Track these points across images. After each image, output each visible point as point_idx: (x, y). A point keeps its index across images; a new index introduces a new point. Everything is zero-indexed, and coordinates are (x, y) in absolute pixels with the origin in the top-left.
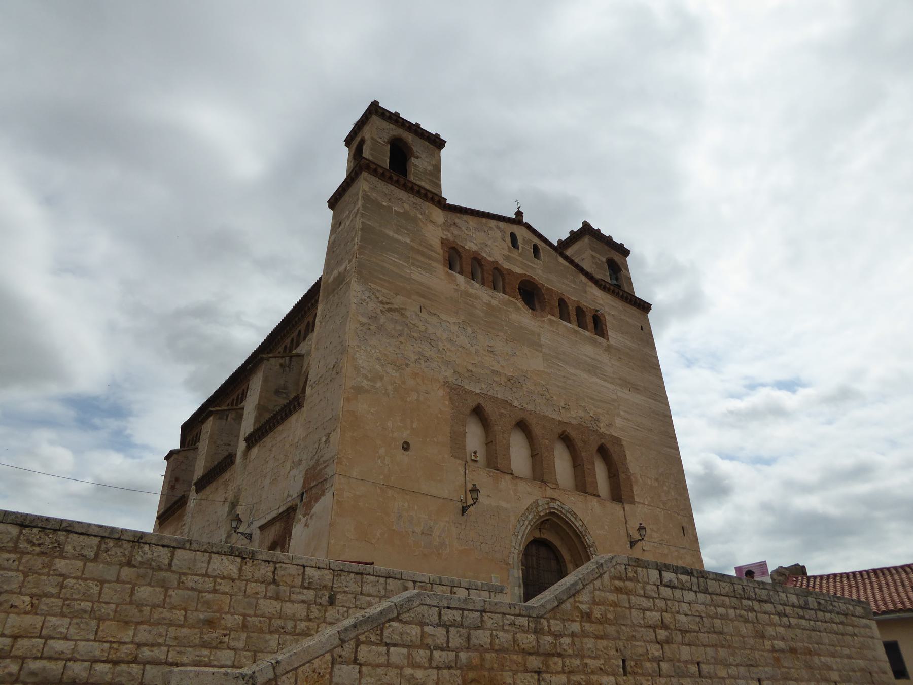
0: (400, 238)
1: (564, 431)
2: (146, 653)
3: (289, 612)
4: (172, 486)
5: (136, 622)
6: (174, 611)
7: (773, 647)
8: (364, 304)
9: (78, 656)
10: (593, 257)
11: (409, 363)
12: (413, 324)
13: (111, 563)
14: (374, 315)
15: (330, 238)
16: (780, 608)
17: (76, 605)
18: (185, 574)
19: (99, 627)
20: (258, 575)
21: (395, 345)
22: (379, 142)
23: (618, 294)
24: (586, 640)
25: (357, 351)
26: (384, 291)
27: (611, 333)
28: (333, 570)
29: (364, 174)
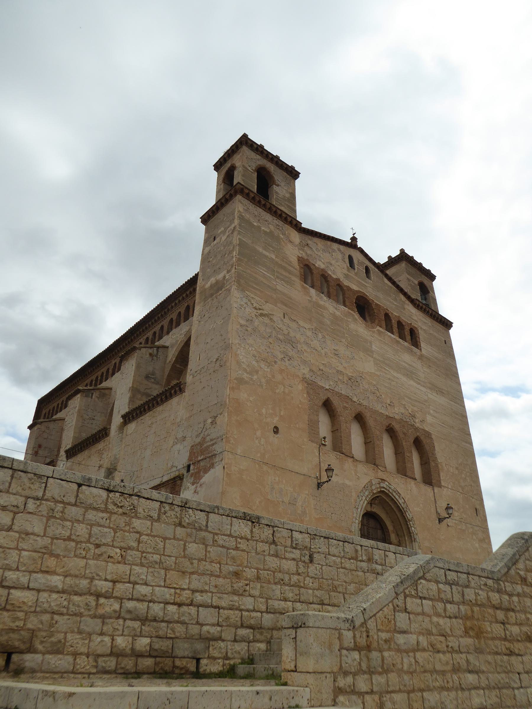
0: (267, 254)
1: (390, 424)
2: (199, 598)
3: (286, 567)
4: (35, 451)
5: (189, 572)
6: (214, 565)
8: (243, 309)
9: (156, 599)
11: (277, 360)
12: (279, 328)
13: (169, 523)
14: (251, 319)
15: (203, 250)
17: (150, 557)
18: (217, 534)
19: (166, 575)
20: (263, 537)
21: (266, 345)
22: (250, 171)
23: (428, 312)
24: (526, 599)
25: (238, 348)
26: (257, 298)
27: (423, 345)
28: (310, 534)
29: (239, 197)
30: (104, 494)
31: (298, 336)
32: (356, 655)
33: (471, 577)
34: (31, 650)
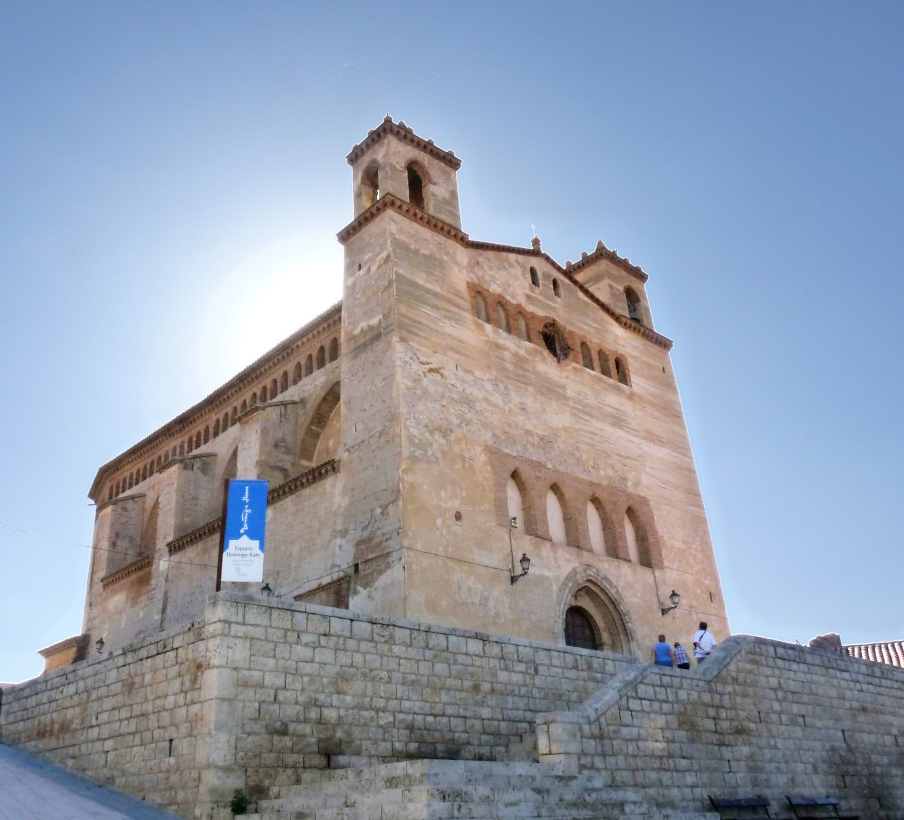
7: (851, 706)
10: (611, 286)
14: (418, 377)
16: (854, 676)
25: (408, 419)
26: (423, 349)
27: (634, 378)
30: (369, 626)
31: (476, 392)
32: (593, 742)
33: (684, 680)
34: (341, 753)
